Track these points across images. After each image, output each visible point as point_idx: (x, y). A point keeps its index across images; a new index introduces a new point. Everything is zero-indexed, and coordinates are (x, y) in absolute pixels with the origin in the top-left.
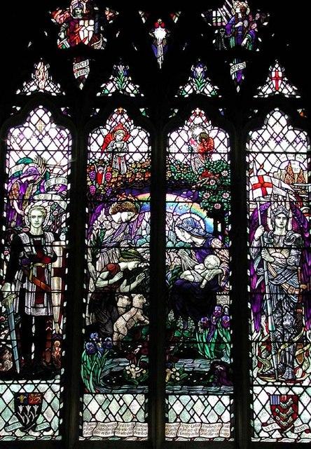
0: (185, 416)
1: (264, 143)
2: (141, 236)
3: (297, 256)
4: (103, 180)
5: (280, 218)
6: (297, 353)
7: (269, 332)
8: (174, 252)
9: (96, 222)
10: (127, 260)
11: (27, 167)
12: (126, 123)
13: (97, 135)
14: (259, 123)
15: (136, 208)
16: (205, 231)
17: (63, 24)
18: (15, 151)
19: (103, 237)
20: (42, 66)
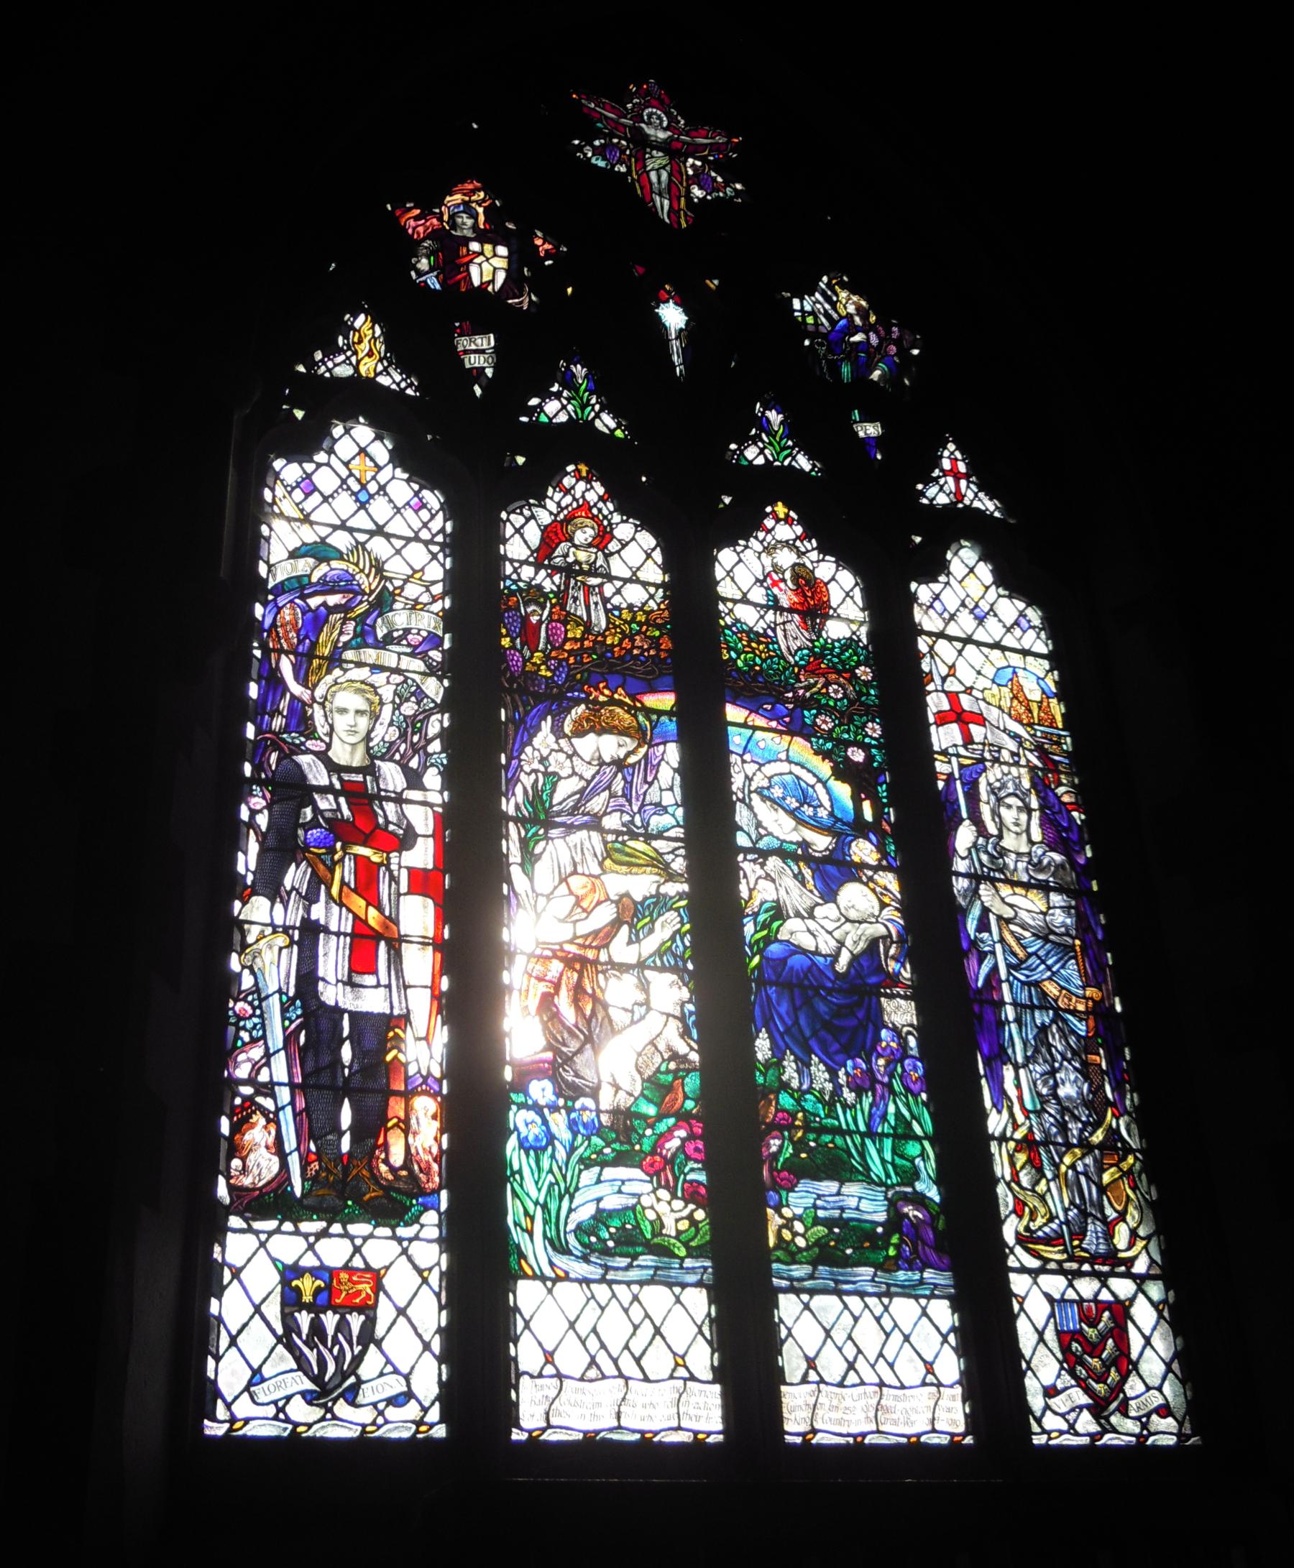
0: (832, 1366)
1: (946, 615)
2: (660, 808)
3: (1067, 909)
4: (542, 640)
5: (1009, 807)
6: (1106, 1178)
7: (1026, 1113)
8: (754, 861)
9: (528, 750)
10: (624, 869)
11: (324, 568)
12: (600, 505)
13: (522, 520)
14: (934, 568)
15: (640, 728)
16: (831, 814)
17: (424, 240)
18: (289, 519)
19: (551, 796)
20: (369, 324)
